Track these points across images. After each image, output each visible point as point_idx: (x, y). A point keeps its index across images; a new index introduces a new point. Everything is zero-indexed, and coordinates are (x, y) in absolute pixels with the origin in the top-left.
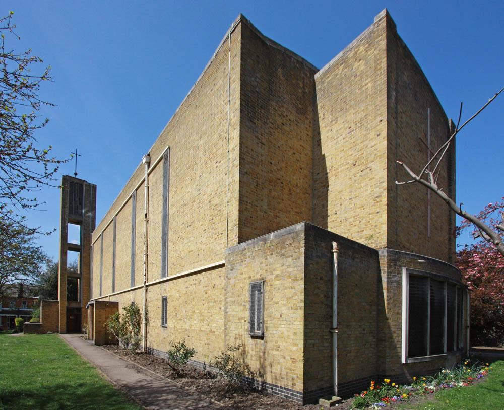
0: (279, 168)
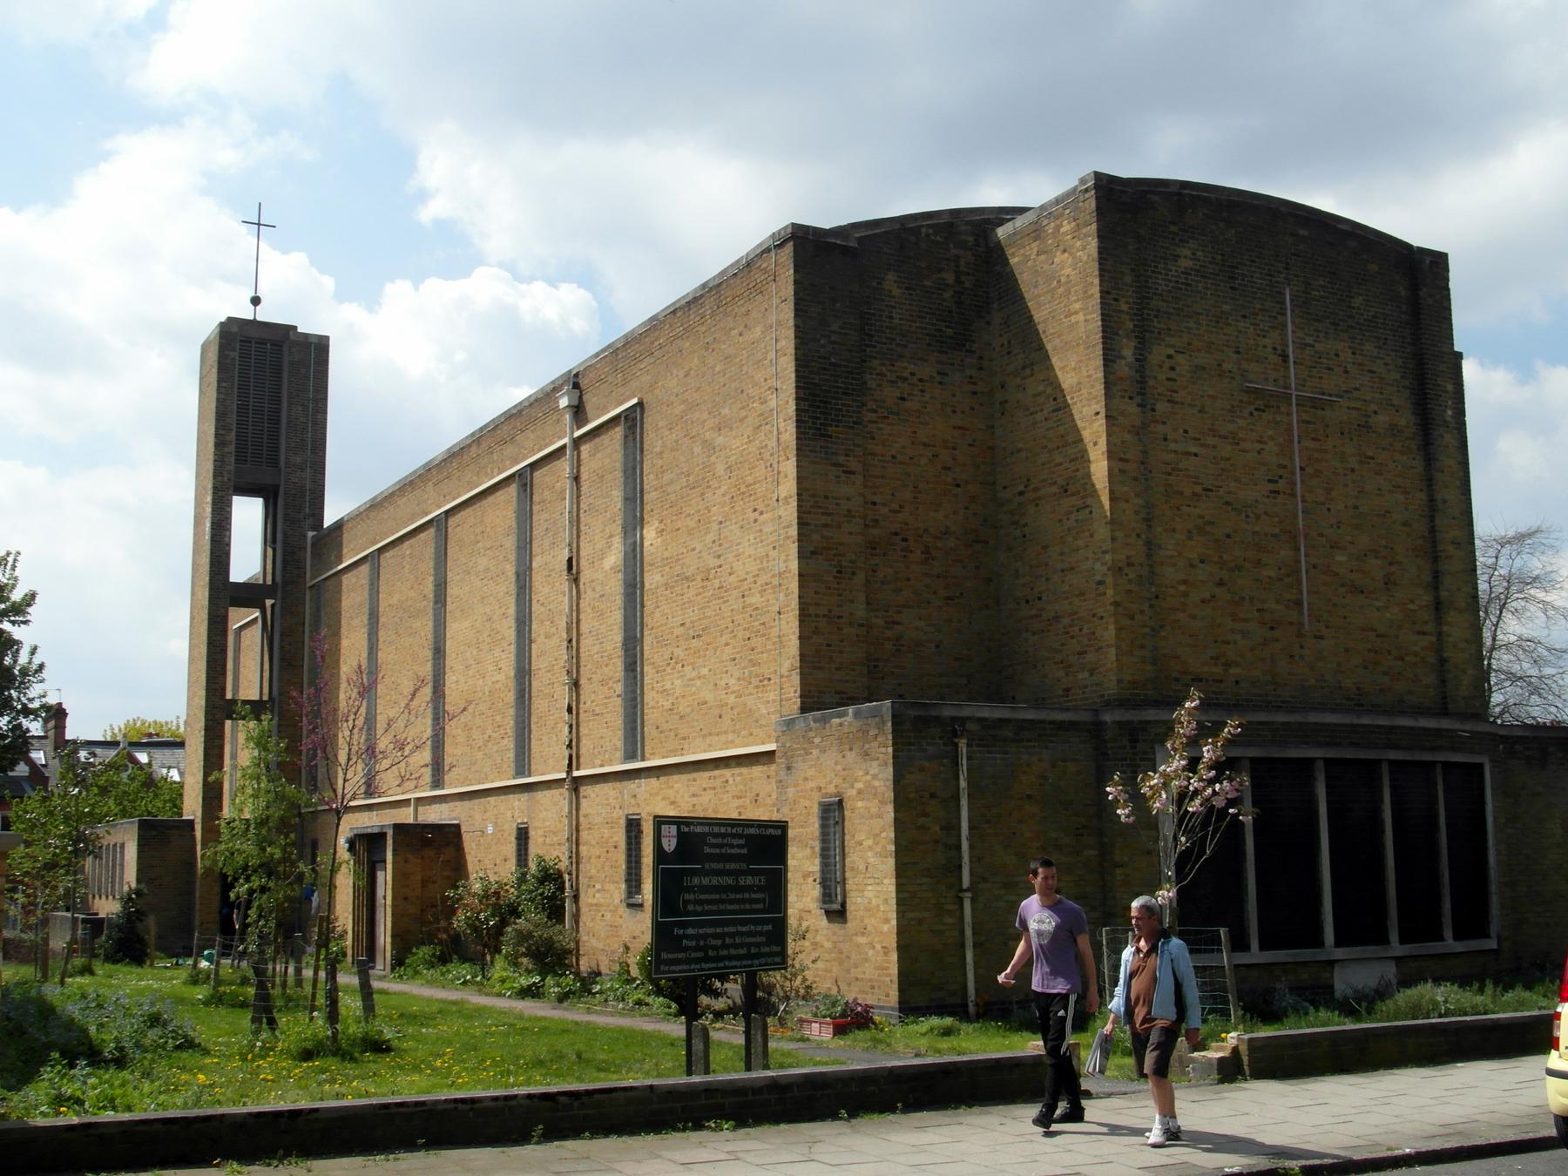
0: (895, 506)
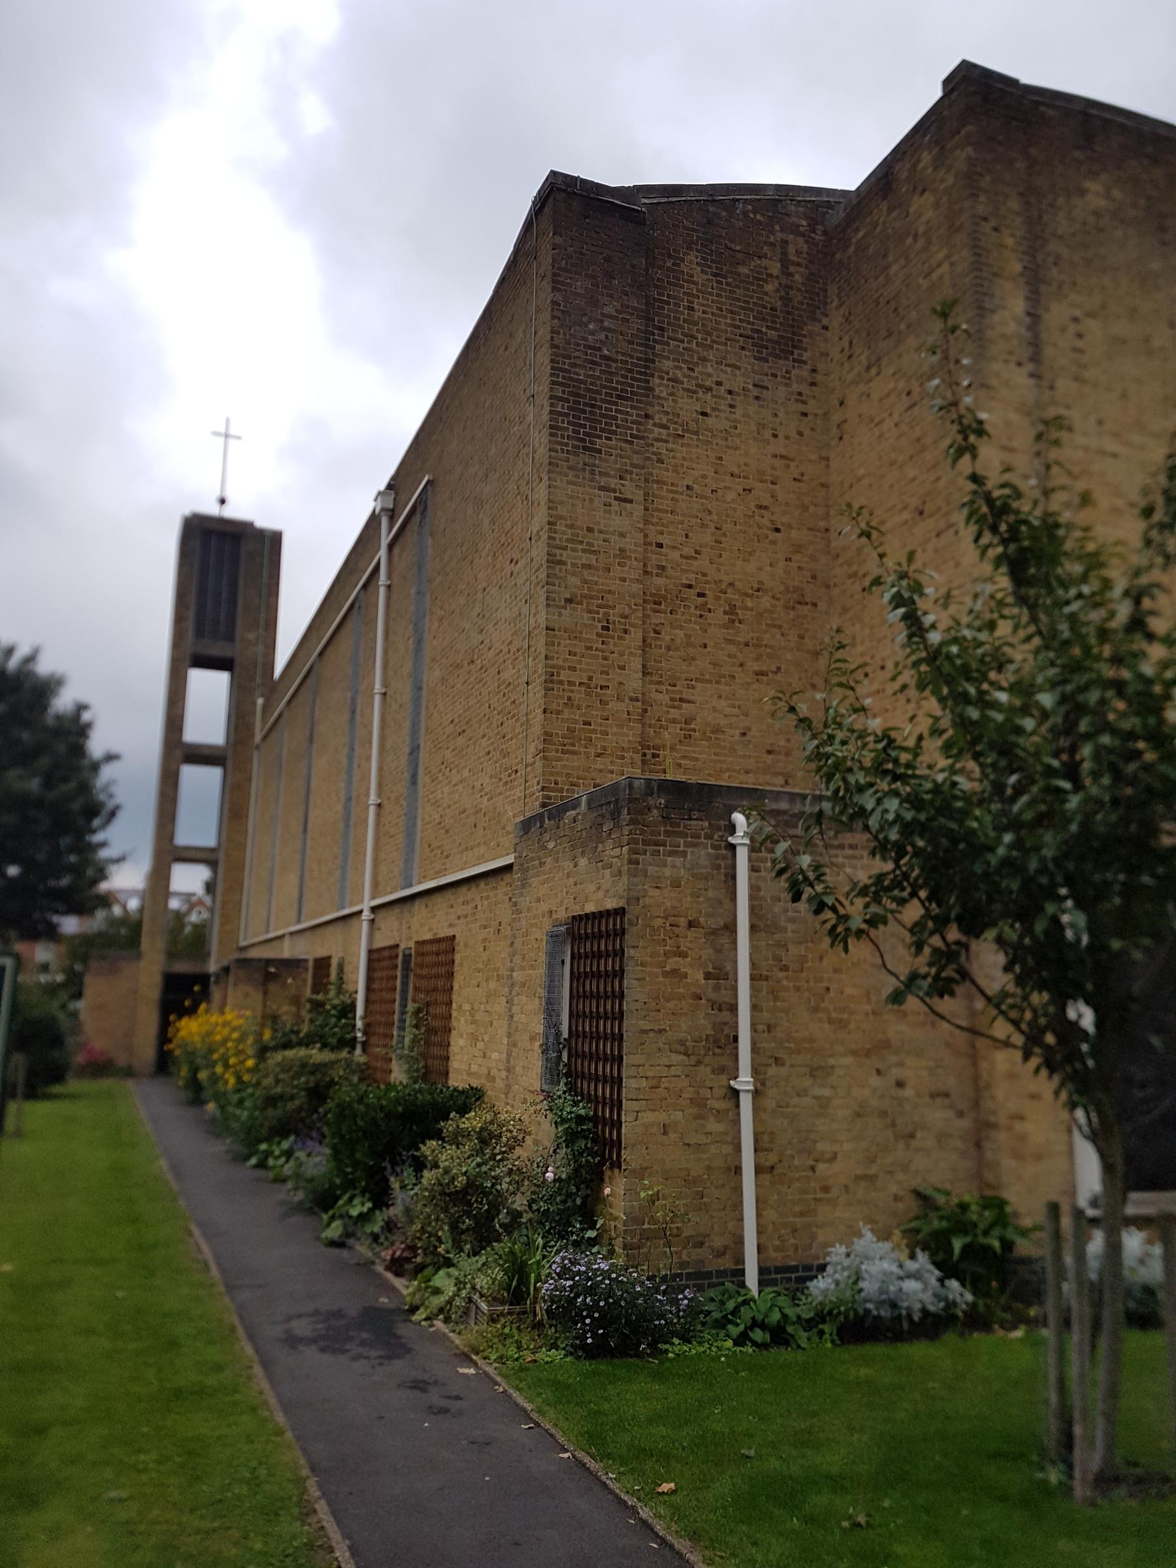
0: (687, 551)
